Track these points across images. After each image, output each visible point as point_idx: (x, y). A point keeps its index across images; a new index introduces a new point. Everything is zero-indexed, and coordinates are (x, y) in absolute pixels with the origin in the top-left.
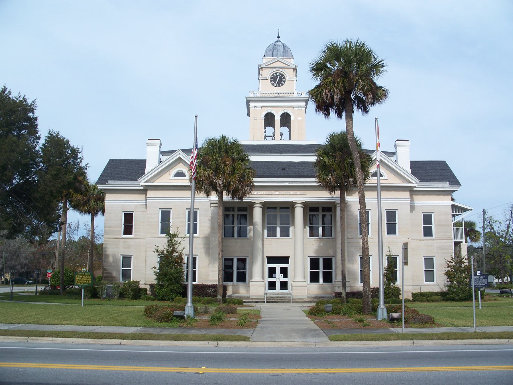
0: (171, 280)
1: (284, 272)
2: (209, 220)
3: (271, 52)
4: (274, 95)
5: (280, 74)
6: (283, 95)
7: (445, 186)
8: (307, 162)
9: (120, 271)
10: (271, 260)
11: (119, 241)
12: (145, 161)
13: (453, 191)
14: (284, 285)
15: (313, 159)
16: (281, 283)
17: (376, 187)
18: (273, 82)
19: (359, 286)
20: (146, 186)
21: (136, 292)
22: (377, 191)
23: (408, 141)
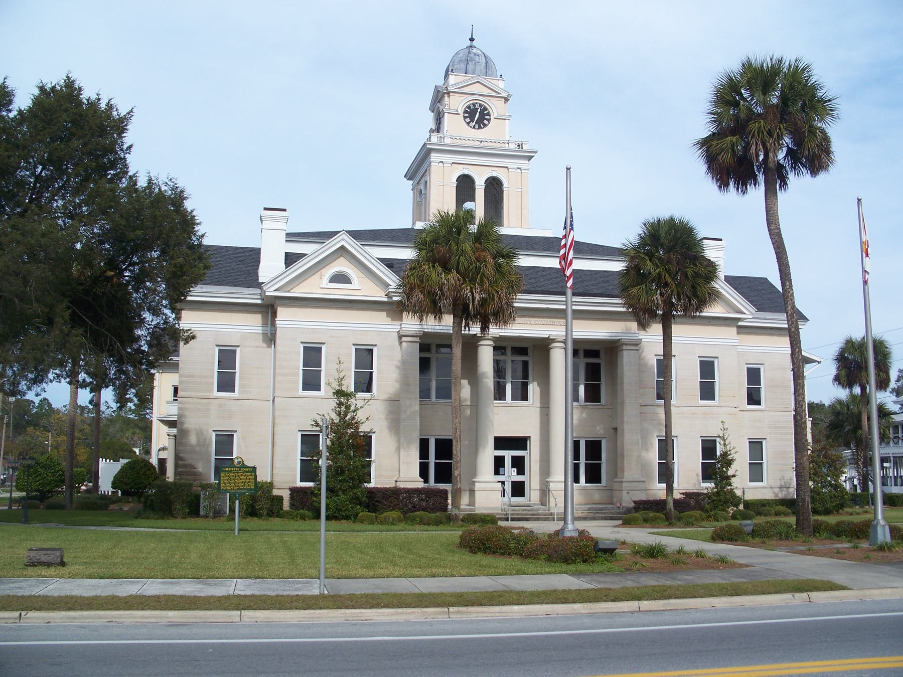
0: (353, 479)
1: (519, 464)
2: (397, 367)
3: (463, 66)
4: (472, 143)
5: (481, 105)
6: (490, 144)
9: (210, 462)
10: (502, 443)
11: (209, 404)
12: (259, 249)
15: (617, 266)
16: (514, 484)
17: (564, 311)
18: (468, 120)
19: (658, 490)
21: (260, 503)
22: (566, 318)
23: (721, 240)
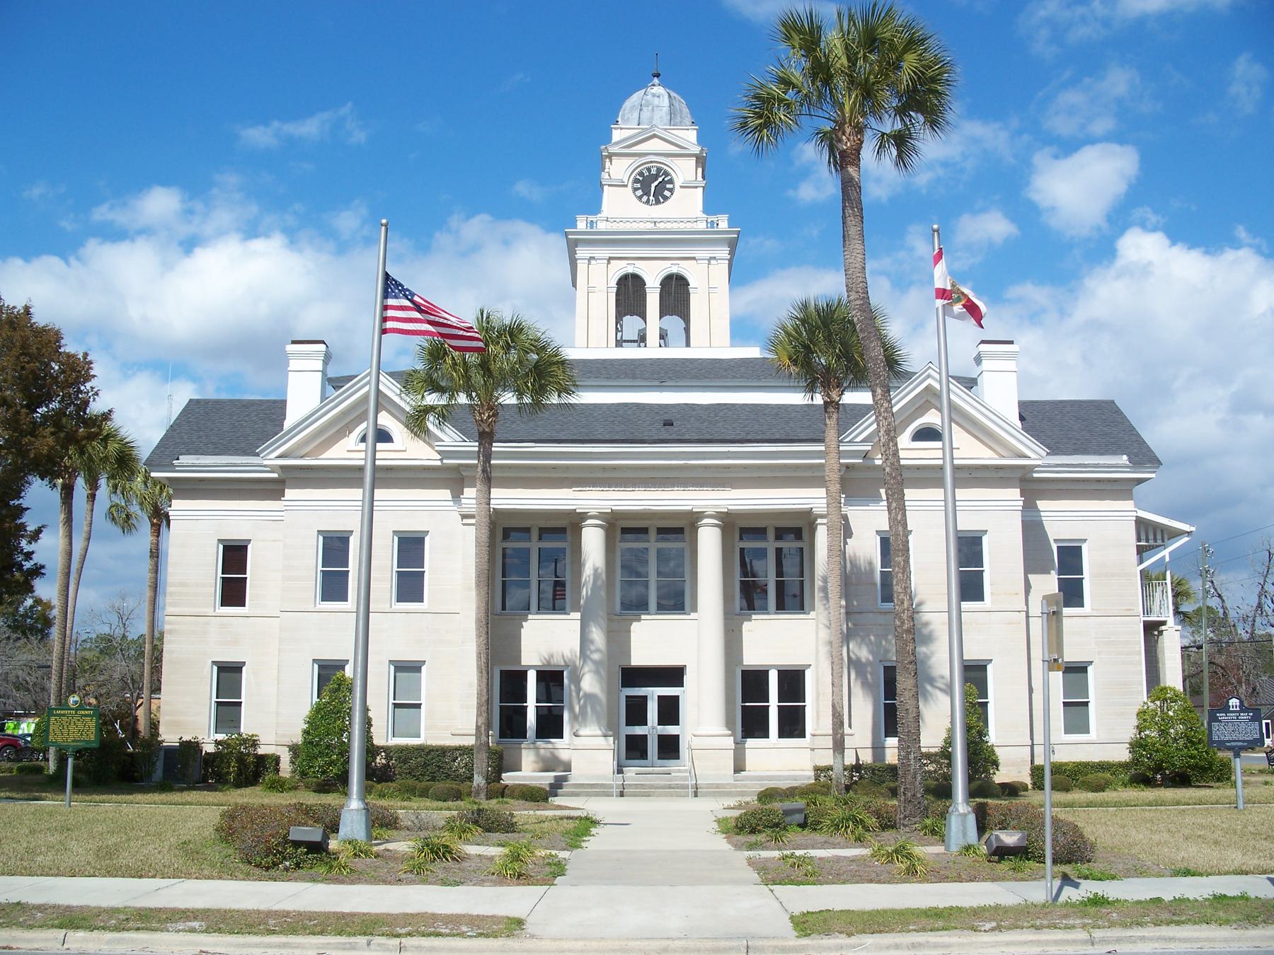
1: (670, 711)
3: (636, 115)
7: (1116, 465)
8: (733, 405)
13: (1140, 481)
14: (670, 747)
18: (639, 193)
20: (283, 467)
